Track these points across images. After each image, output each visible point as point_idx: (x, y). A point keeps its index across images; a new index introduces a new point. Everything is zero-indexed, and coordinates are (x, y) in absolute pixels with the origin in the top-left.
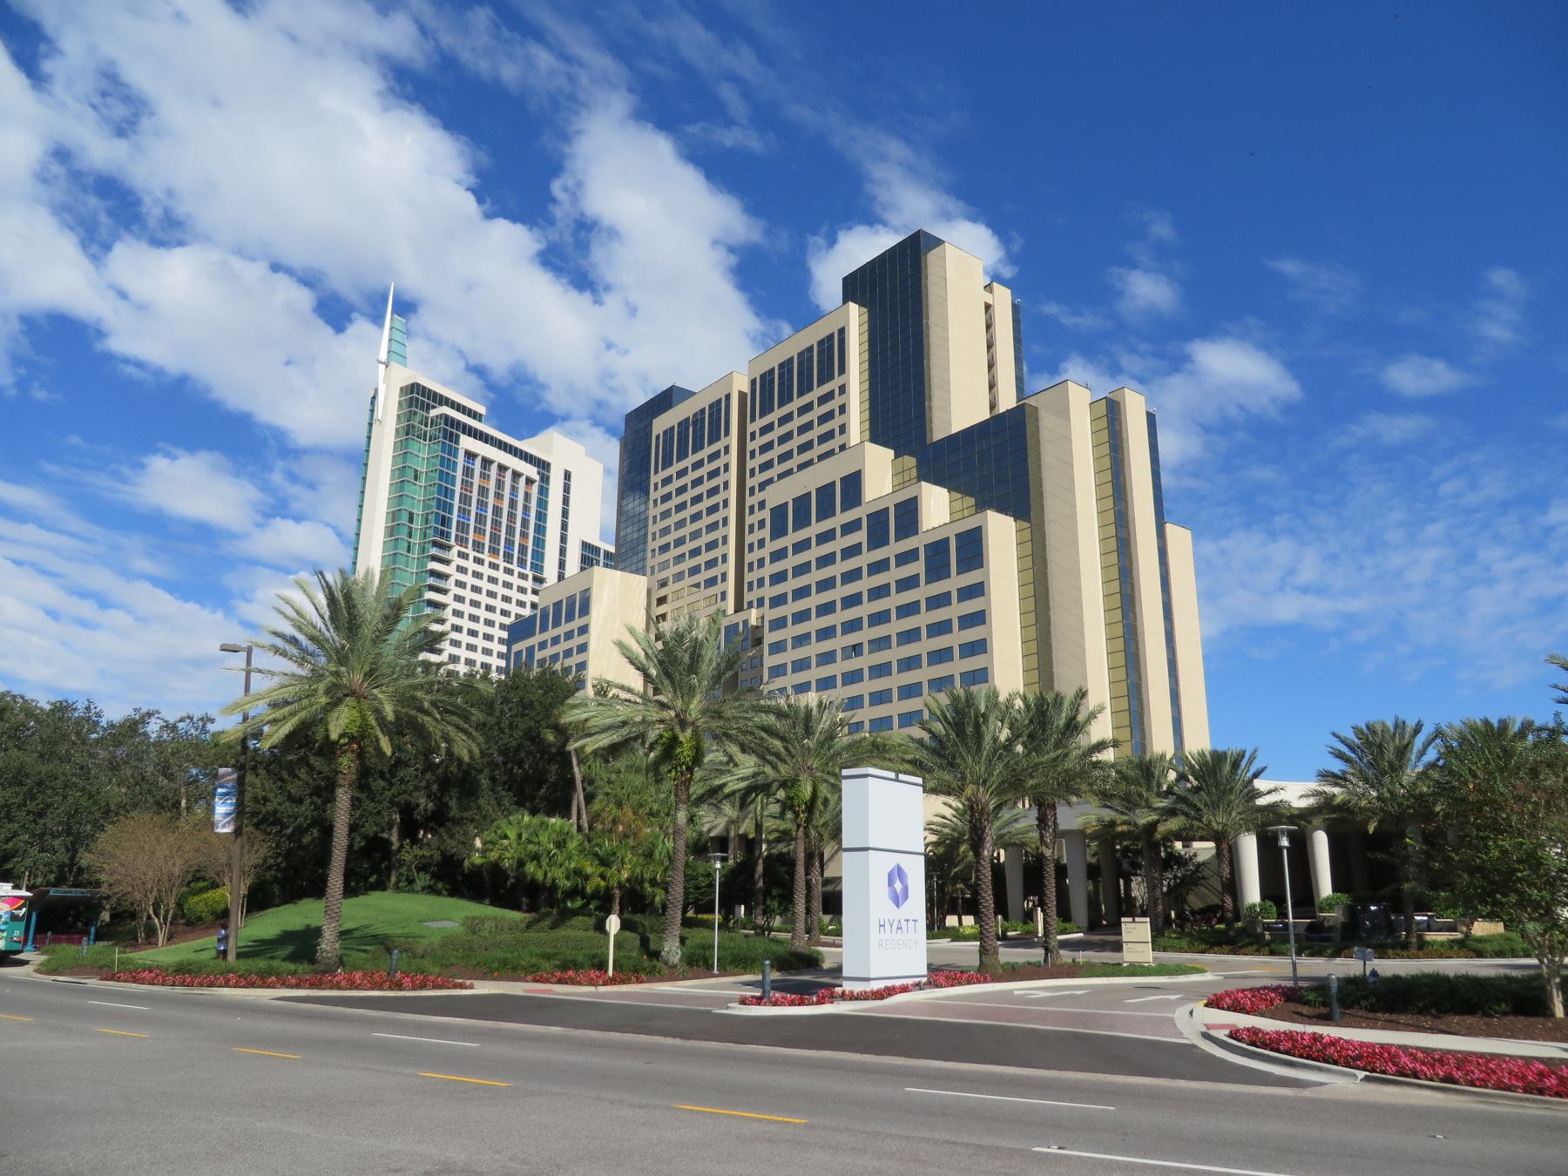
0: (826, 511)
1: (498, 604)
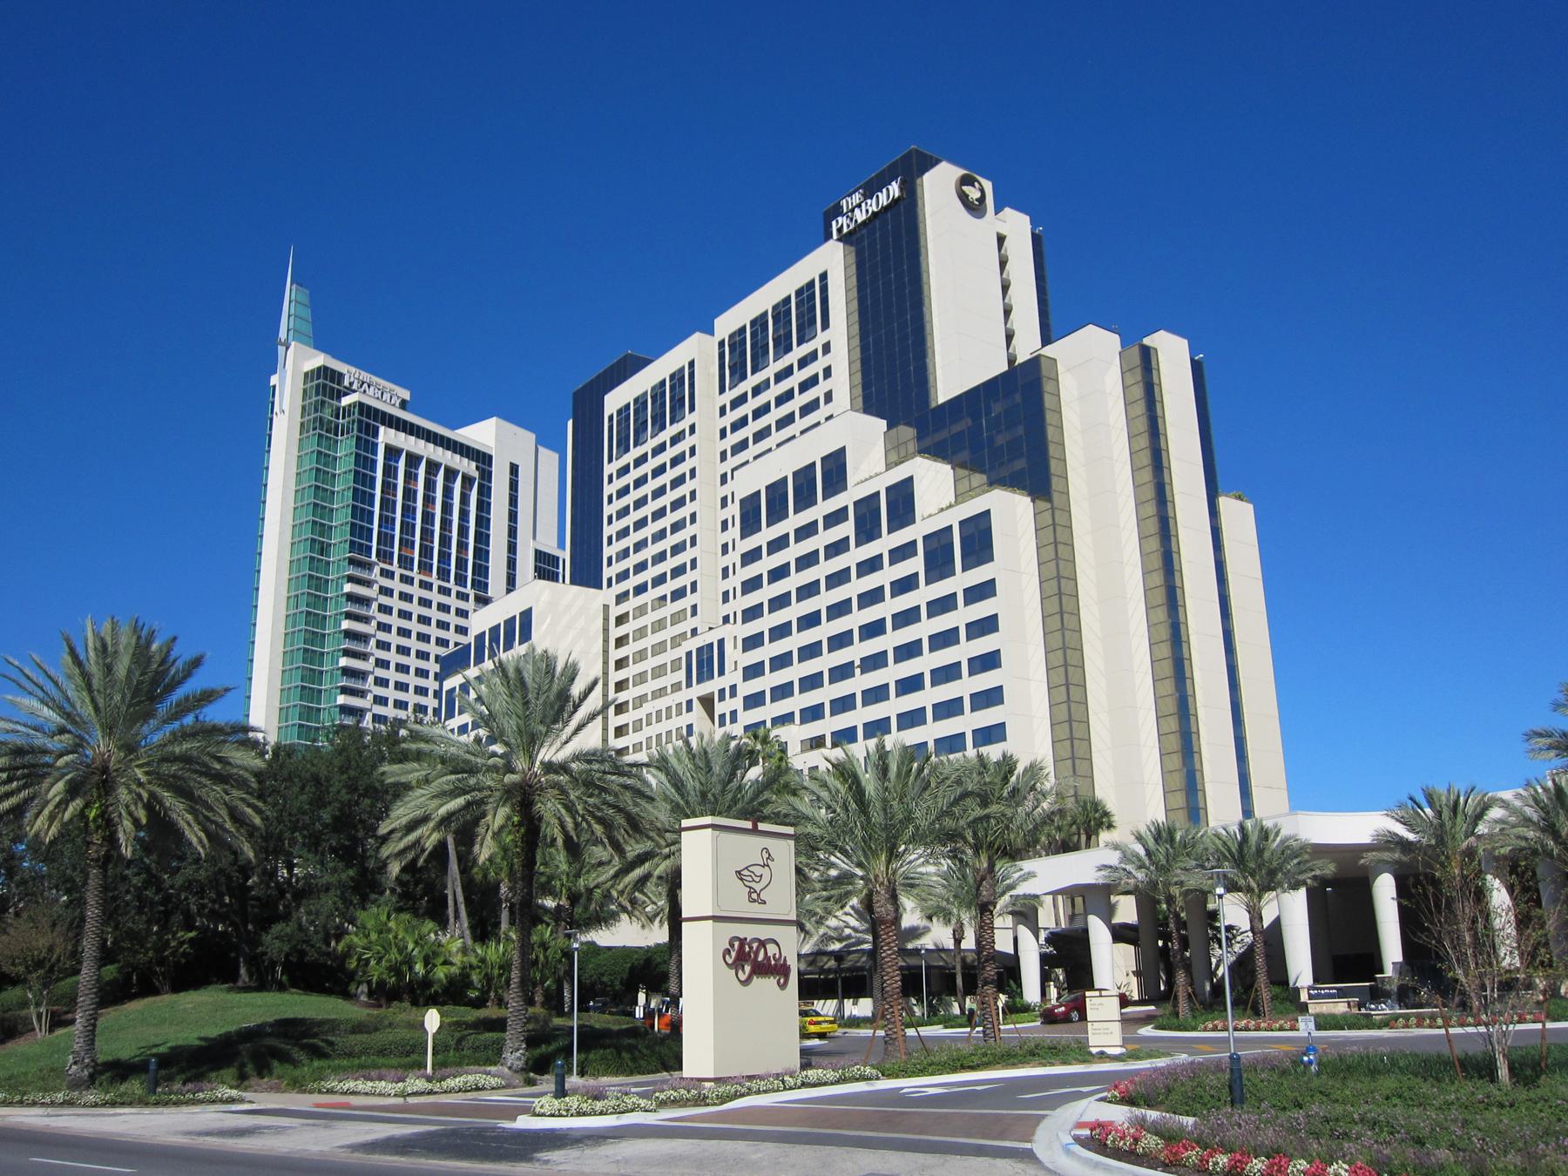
0: (805, 498)
1: (433, 631)
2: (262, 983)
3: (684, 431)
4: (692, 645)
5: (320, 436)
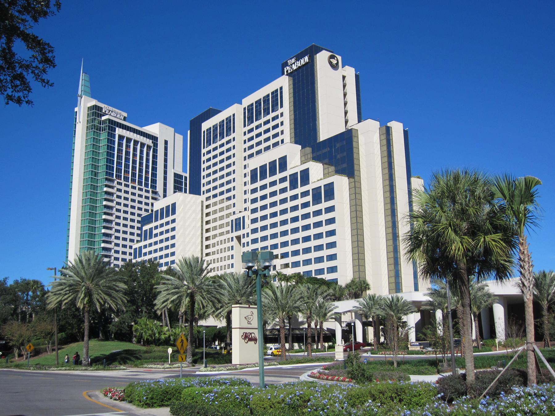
0: (273, 172)
2: (107, 338)
3: (231, 139)
4: (233, 217)
5: (94, 132)
